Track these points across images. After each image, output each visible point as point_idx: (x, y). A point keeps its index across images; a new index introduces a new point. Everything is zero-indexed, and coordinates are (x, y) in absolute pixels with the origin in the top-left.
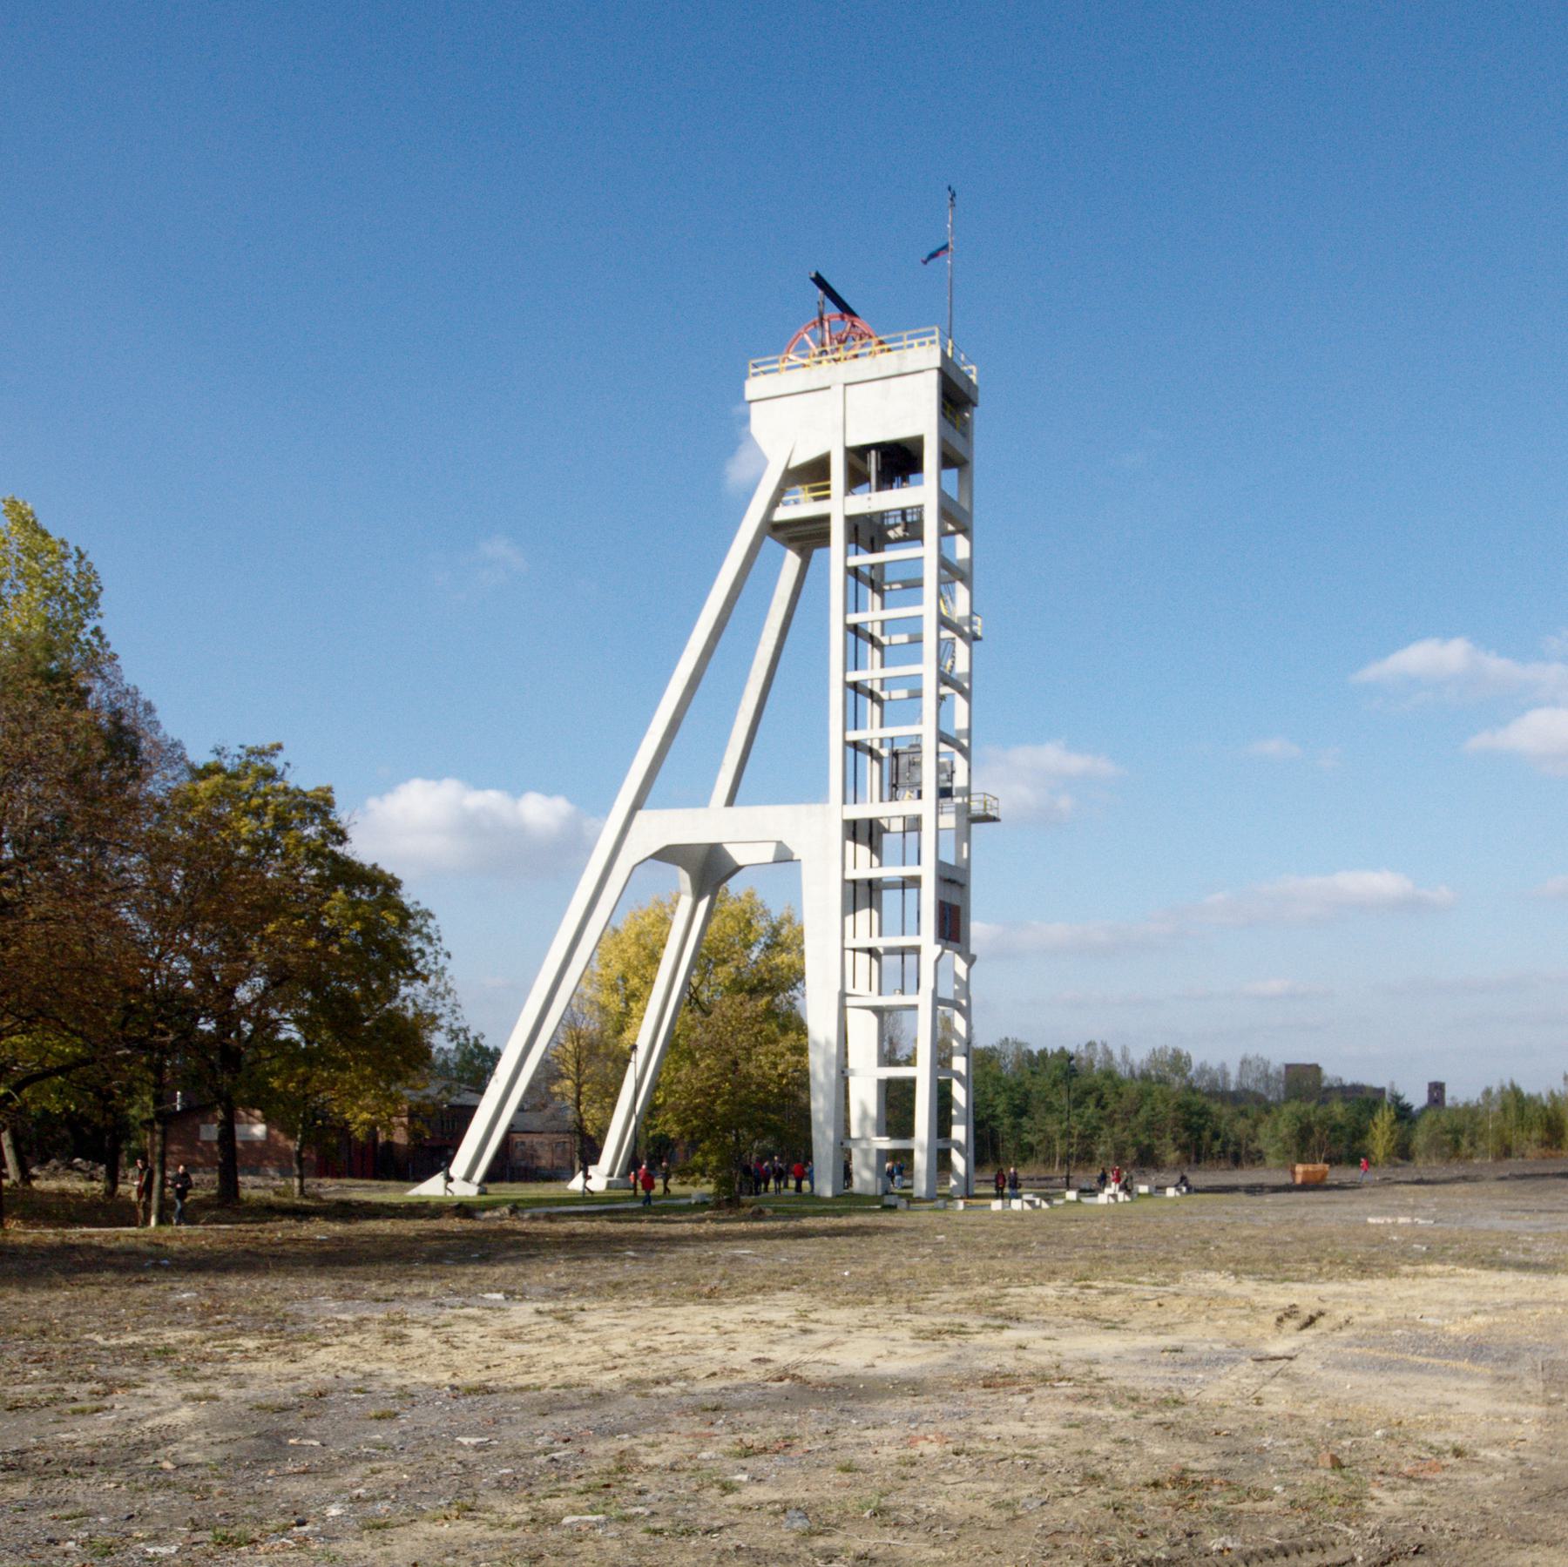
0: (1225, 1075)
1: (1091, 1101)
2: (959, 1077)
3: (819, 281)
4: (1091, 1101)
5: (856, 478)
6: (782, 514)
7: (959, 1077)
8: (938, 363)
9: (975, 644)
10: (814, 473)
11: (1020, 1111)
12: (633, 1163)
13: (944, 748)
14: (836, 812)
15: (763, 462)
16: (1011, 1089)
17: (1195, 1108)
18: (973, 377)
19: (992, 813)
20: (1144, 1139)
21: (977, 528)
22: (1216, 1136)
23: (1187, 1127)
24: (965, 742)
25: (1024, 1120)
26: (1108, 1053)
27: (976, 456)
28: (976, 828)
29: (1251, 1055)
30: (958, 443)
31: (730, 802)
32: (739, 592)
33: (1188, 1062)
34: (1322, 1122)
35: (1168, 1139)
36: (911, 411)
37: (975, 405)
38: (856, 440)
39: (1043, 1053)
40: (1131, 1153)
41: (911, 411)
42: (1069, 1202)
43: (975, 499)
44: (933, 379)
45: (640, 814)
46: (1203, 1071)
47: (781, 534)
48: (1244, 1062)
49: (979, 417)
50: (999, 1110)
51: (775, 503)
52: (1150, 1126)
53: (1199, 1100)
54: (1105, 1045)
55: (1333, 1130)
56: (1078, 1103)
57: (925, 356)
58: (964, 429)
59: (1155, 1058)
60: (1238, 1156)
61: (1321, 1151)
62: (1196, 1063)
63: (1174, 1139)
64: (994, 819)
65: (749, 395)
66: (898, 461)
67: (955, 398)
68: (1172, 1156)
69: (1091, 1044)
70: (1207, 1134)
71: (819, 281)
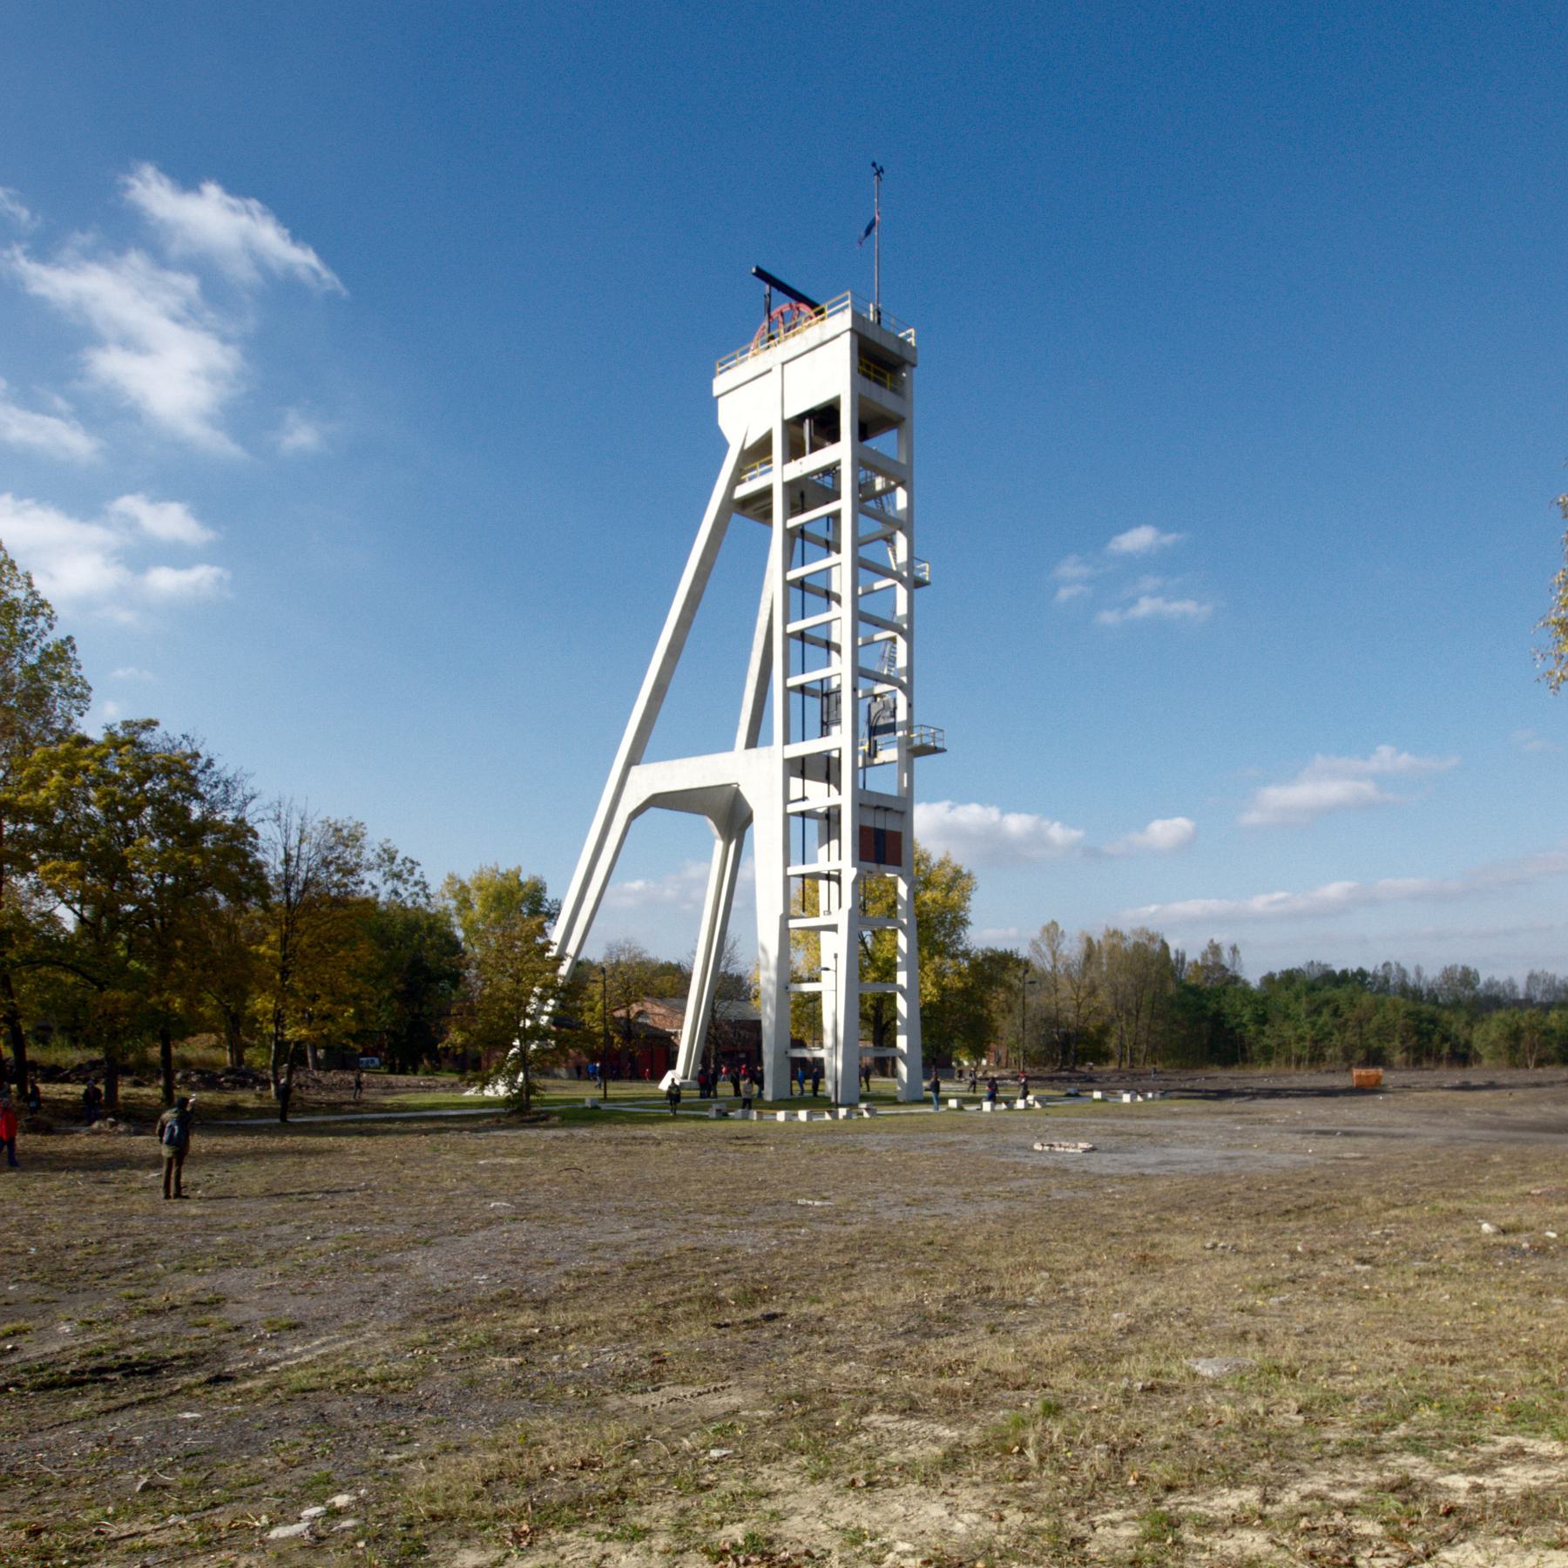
0: (1513, 987)
1: (1326, 1012)
2: (902, 991)
3: (761, 274)
4: (1326, 1012)
5: (794, 450)
7: (902, 991)
8: (849, 325)
9: (918, 592)
10: (759, 452)
11: (1262, 1020)
12: (704, 1059)
14: (775, 754)
15: (725, 446)
16: (1256, 1002)
17: (1424, 1015)
18: (912, 340)
19: (939, 745)
20: (1374, 1043)
21: (918, 480)
22: (1445, 1039)
23: (1419, 1033)
24: (904, 679)
25: (1266, 1028)
26: (1404, 973)
27: (916, 414)
28: (919, 762)
29: (1537, 971)
32: (710, 568)
33: (1477, 978)
34: (1532, 1028)
35: (1397, 1043)
37: (914, 366)
38: (791, 413)
39: (1344, 972)
40: (1360, 1054)
42: (950, 1109)
43: (916, 452)
44: (846, 341)
45: (634, 770)
46: (1490, 984)
47: (749, 511)
48: (1532, 978)
49: (918, 380)
50: (1245, 1019)
51: (736, 480)
52: (1379, 1032)
53: (1427, 1008)
54: (1398, 965)
55: (1545, 1033)
56: (1317, 1011)
57: (840, 322)
59: (1448, 974)
60: (1463, 1056)
61: (1531, 1052)
62: (1483, 978)
63: (1402, 1043)
64: (936, 750)
65: (716, 393)
66: (823, 421)
67: (876, 361)
68: (1398, 1057)
69: (1386, 965)
70: (1436, 1038)
71: (761, 274)
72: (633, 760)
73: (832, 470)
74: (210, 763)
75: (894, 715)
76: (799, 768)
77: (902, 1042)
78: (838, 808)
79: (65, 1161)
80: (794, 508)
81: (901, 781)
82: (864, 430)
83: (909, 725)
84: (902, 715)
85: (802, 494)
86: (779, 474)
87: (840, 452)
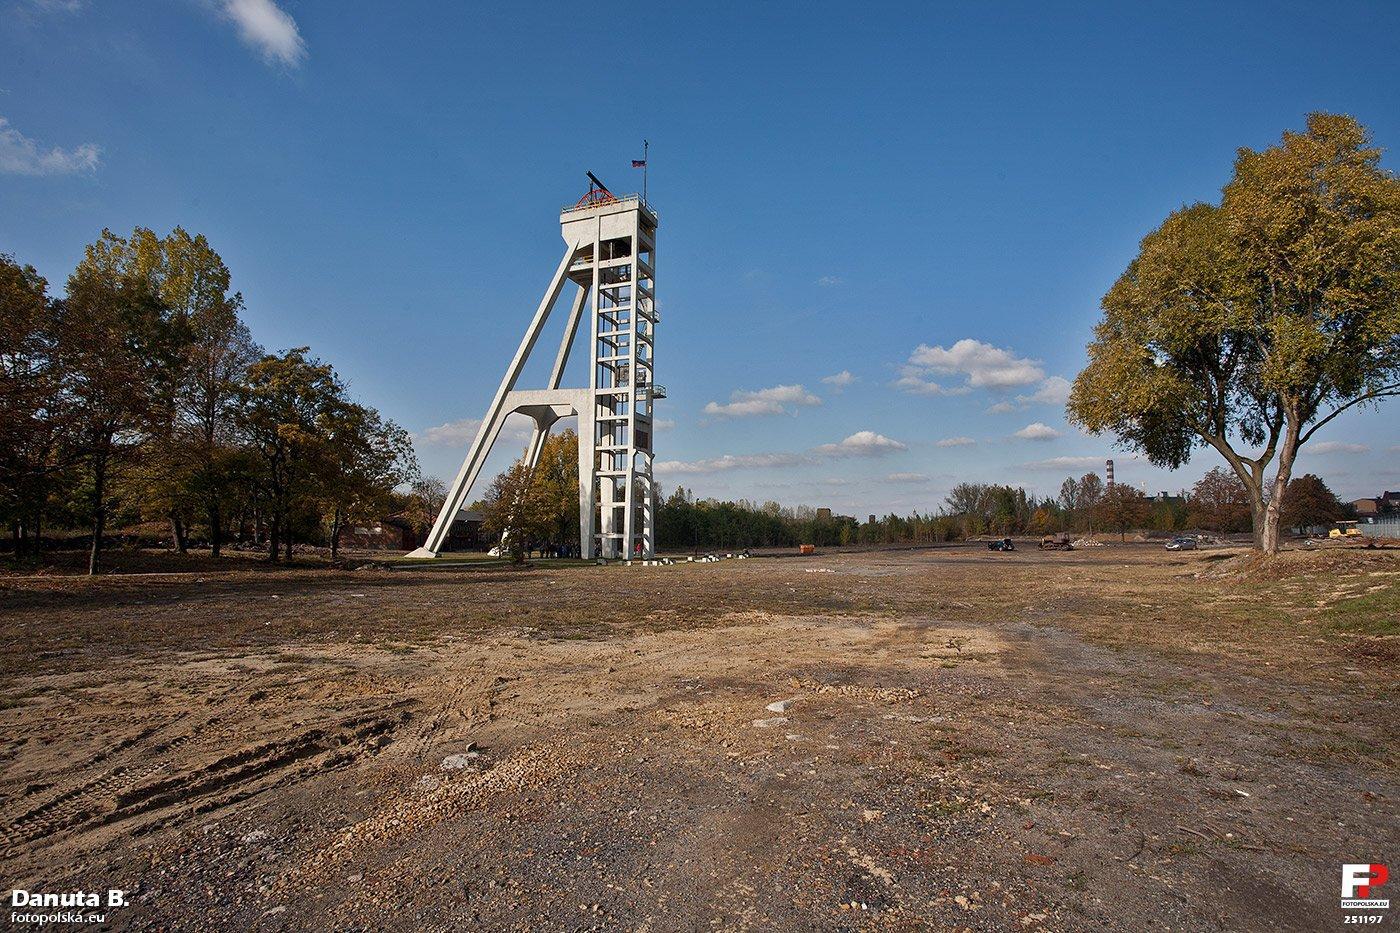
3: (590, 174)
5: (604, 256)
6: (573, 268)
10: (586, 252)
13: (639, 366)
14: (593, 392)
30: (647, 240)
31: (556, 387)
36: (624, 224)
41: (624, 224)
49: (658, 232)
51: (571, 263)
58: (652, 237)
59: (1069, 487)
66: (621, 247)
67: (646, 223)
71: (590, 174)
72: (509, 389)
73: (627, 266)
74: (1071, 398)
75: (644, 379)
76: (601, 400)
77: (646, 531)
78: (627, 420)
79: (37, 603)
80: (602, 281)
81: (648, 410)
82: (642, 248)
83: (651, 384)
84: (648, 380)
85: (607, 276)
86: (597, 265)
87: (632, 260)
